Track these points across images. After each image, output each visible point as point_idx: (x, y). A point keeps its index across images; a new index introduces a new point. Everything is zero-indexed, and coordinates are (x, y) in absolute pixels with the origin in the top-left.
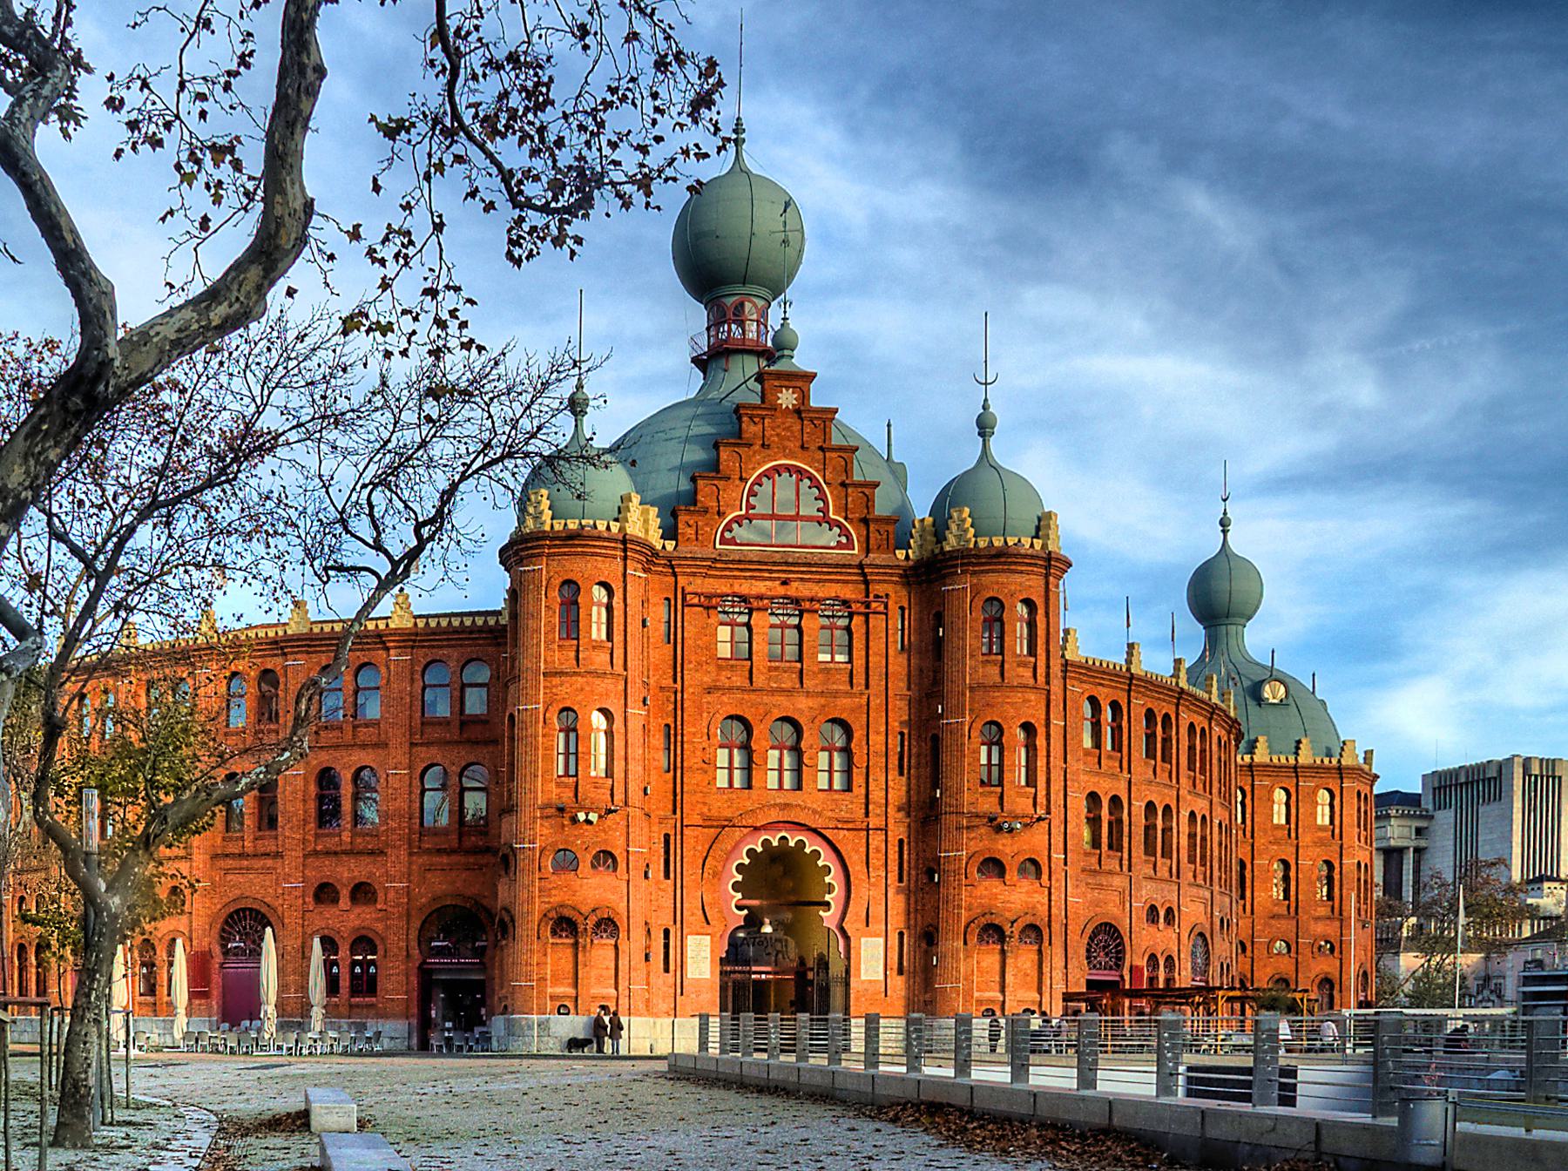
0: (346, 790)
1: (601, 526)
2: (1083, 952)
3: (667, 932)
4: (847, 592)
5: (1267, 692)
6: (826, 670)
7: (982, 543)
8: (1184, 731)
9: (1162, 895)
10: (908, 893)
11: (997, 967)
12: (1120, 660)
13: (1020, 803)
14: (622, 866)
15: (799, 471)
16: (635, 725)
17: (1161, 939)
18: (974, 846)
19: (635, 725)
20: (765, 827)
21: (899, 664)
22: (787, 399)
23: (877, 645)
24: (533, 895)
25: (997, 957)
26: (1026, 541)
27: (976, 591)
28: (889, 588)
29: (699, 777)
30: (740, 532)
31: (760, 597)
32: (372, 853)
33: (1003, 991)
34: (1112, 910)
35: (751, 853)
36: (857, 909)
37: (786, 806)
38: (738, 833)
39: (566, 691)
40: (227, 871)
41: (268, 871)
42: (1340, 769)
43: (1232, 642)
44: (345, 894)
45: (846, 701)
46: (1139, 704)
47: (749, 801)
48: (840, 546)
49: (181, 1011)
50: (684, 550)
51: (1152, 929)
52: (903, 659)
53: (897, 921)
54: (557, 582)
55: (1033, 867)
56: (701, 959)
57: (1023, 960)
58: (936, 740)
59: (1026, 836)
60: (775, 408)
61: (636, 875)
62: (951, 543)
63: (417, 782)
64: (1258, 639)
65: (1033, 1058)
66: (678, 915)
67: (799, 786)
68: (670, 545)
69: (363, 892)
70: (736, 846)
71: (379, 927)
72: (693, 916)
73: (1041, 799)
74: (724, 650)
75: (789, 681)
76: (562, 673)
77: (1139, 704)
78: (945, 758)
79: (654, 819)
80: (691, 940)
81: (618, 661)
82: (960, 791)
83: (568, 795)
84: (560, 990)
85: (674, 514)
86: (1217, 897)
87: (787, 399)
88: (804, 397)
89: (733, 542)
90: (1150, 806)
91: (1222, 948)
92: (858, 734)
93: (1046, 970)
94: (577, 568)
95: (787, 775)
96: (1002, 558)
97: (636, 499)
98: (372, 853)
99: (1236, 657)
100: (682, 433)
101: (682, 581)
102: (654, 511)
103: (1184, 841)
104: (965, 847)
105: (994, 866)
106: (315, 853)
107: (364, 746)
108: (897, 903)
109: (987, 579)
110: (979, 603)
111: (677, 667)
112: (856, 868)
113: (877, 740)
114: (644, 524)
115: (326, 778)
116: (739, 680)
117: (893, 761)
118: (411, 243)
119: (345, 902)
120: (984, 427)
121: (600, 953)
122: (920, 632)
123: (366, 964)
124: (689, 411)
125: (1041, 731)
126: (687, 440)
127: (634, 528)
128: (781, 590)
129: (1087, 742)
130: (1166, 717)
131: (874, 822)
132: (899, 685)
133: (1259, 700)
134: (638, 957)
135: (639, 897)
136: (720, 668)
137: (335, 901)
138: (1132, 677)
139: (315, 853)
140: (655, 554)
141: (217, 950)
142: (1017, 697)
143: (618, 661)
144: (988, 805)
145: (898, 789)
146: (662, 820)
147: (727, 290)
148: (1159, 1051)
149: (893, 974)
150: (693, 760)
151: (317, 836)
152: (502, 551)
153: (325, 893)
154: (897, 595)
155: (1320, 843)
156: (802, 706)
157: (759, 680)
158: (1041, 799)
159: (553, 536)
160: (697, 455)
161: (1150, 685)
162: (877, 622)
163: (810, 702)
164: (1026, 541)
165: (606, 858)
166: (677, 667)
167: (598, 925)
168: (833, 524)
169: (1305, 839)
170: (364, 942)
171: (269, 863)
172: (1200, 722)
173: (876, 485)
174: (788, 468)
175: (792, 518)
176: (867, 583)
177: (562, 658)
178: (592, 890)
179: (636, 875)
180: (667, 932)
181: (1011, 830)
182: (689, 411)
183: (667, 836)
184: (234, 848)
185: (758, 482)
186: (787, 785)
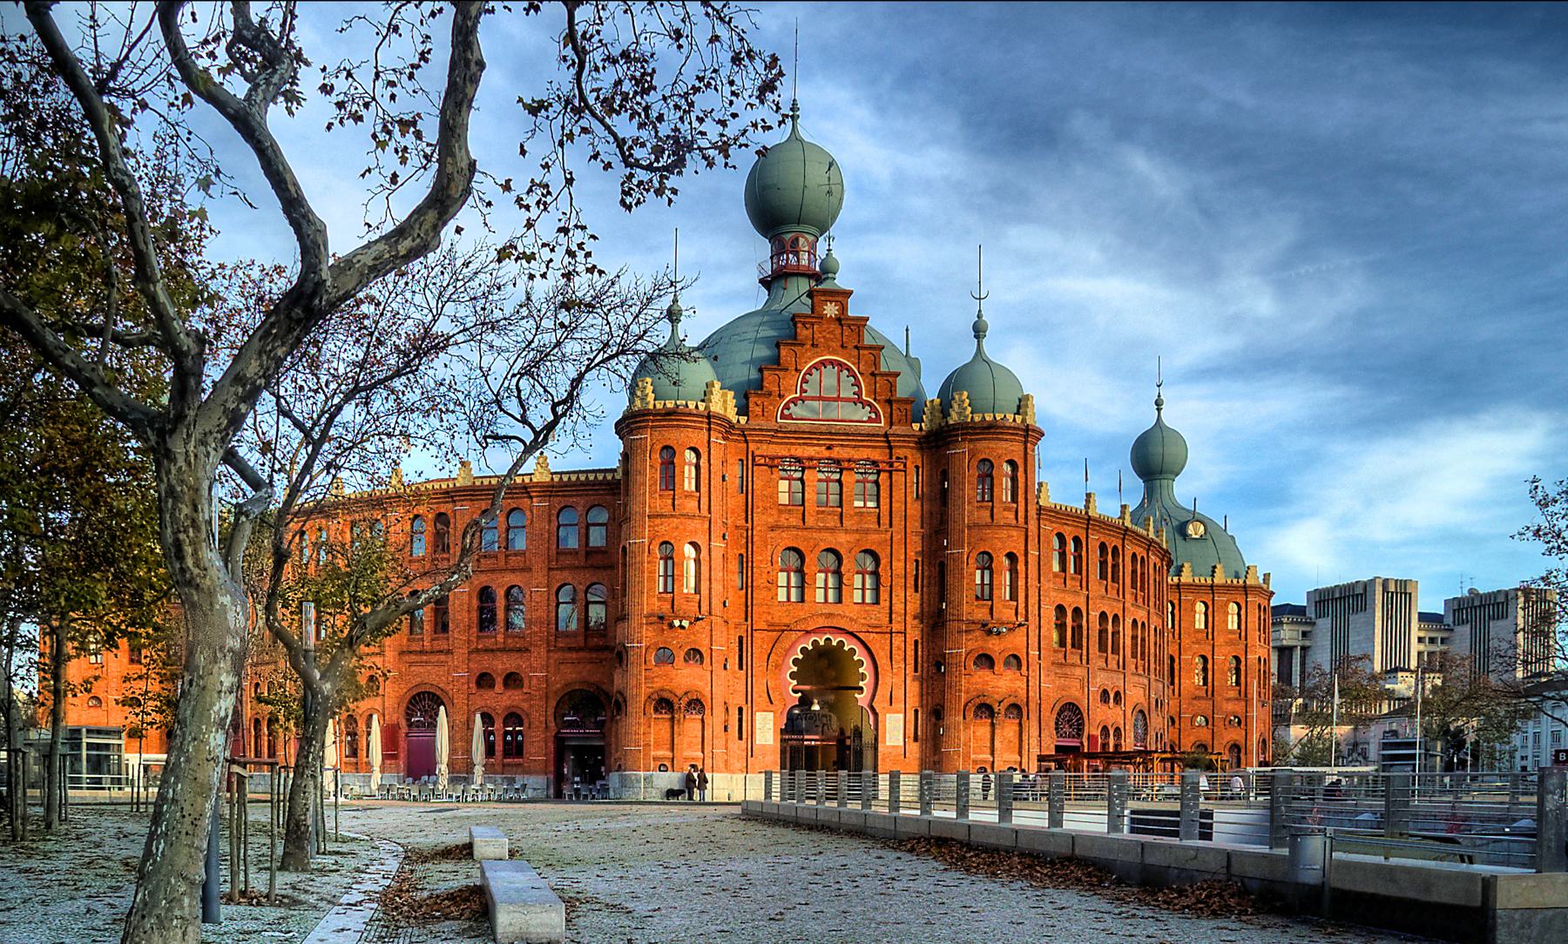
0: (500, 603)
1: (692, 405)
2: (1053, 724)
3: (740, 710)
4: (876, 455)
5: (1191, 530)
6: (860, 513)
7: (977, 418)
8: (1128, 559)
9: (1111, 682)
10: (921, 680)
11: (988, 736)
12: (1081, 505)
13: (1005, 613)
14: (707, 660)
15: (840, 364)
16: (717, 555)
17: (1111, 715)
18: (971, 645)
19: (717, 555)
20: (814, 631)
21: (914, 509)
22: (831, 310)
23: (898, 495)
24: (641, 681)
25: (988, 729)
26: (1010, 417)
27: (972, 455)
28: (907, 452)
29: (764, 593)
30: (795, 410)
31: (811, 459)
32: (519, 650)
33: (992, 754)
34: (1075, 693)
35: (804, 650)
36: (883, 692)
37: (830, 615)
38: (794, 636)
39: (665, 529)
40: (411, 664)
41: (442, 664)
42: (1245, 587)
43: (1165, 492)
44: (499, 681)
45: (875, 537)
46: (1095, 539)
47: (803, 611)
48: (870, 420)
49: (377, 768)
50: (754, 423)
51: (1105, 707)
52: (917, 505)
53: (913, 701)
54: (659, 447)
55: (1015, 661)
56: (766, 729)
57: (1008, 730)
58: (942, 566)
59: (1010, 637)
60: (822, 317)
61: (718, 667)
62: (954, 418)
63: (553, 597)
64: (1182, 491)
65: (1015, 804)
66: (749, 696)
67: (839, 600)
68: (743, 420)
69: (512, 680)
70: (793, 645)
71: (525, 706)
72: (760, 697)
73: (1021, 610)
74: (784, 499)
75: (833, 521)
76: (662, 516)
77: (1095, 539)
78: (949, 579)
79: (731, 625)
80: (758, 716)
81: (704, 506)
82: (960, 604)
83: (666, 607)
84: (660, 753)
85: (746, 397)
86: (1153, 684)
87: (831, 310)
88: (844, 308)
89: (790, 417)
90: (1103, 616)
91: (1157, 722)
92: (884, 562)
93: (1025, 738)
94: (673, 437)
95: (831, 592)
96: (992, 429)
97: (718, 385)
98: (519, 650)
99: (1168, 504)
100: (752, 335)
101: (752, 446)
102: (731, 394)
103: (1128, 642)
104: (964, 646)
105: (986, 660)
106: (477, 651)
107: (513, 570)
108: (913, 688)
109: (982, 445)
110: (975, 463)
111: (748, 511)
112: (883, 661)
113: (898, 566)
114: (724, 404)
115: (485, 594)
116: (795, 521)
117: (911, 581)
118: (549, 193)
119: (499, 687)
120: (979, 331)
121: (690, 726)
122: (930, 485)
123: (515, 734)
124: (758, 319)
125: (1021, 559)
126: (756, 341)
127: (716, 407)
128: (827, 454)
129: (1056, 568)
130: (1115, 548)
131: (896, 627)
132: (915, 525)
133: (1185, 536)
134: (719, 728)
135: (718, 683)
136: (780, 512)
137: (492, 686)
138: (1089, 518)
139: (477, 651)
140: (732, 426)
141: (403, 723)
142: (1003, 534)
143: (704, 506)
144: (981, 614)
145: (914, 605)
146: (737, 626)
147: (785, 229)
148: (1110, 799)
149: (910, 741)
150: (760, 581)
151: (478, 638)
152: (617, 424)
153: (484, 681)
154: (913, 457)
155: (1231, 643)
156: (842, 541)
157: (810, 521)
158: (1021, 610)
159: (656, 413)
160: (763, 352)
161: (1103, 524)
162: (898, 478)
163: (848, 537)
164: (1010, 417)
165: (695, 654)
166: (748, 511)
167: (689, 704)
168: (864, 404)
169: (1219, 640)
170: (513, 717)
171: (443, 657)
172: (1141, 552)
173: (898, 374)
174: (832, 362)
175: (835, 400)
176: (890, 448)
177: (662, 504)
178: (684, 678)
179: (718, 667)
180: (740, 710)
181: (999, 633)
182: (758, 319)
183: (741, 638)
184: (416, 647)
185: (809, 373)
186: (831, 599)
